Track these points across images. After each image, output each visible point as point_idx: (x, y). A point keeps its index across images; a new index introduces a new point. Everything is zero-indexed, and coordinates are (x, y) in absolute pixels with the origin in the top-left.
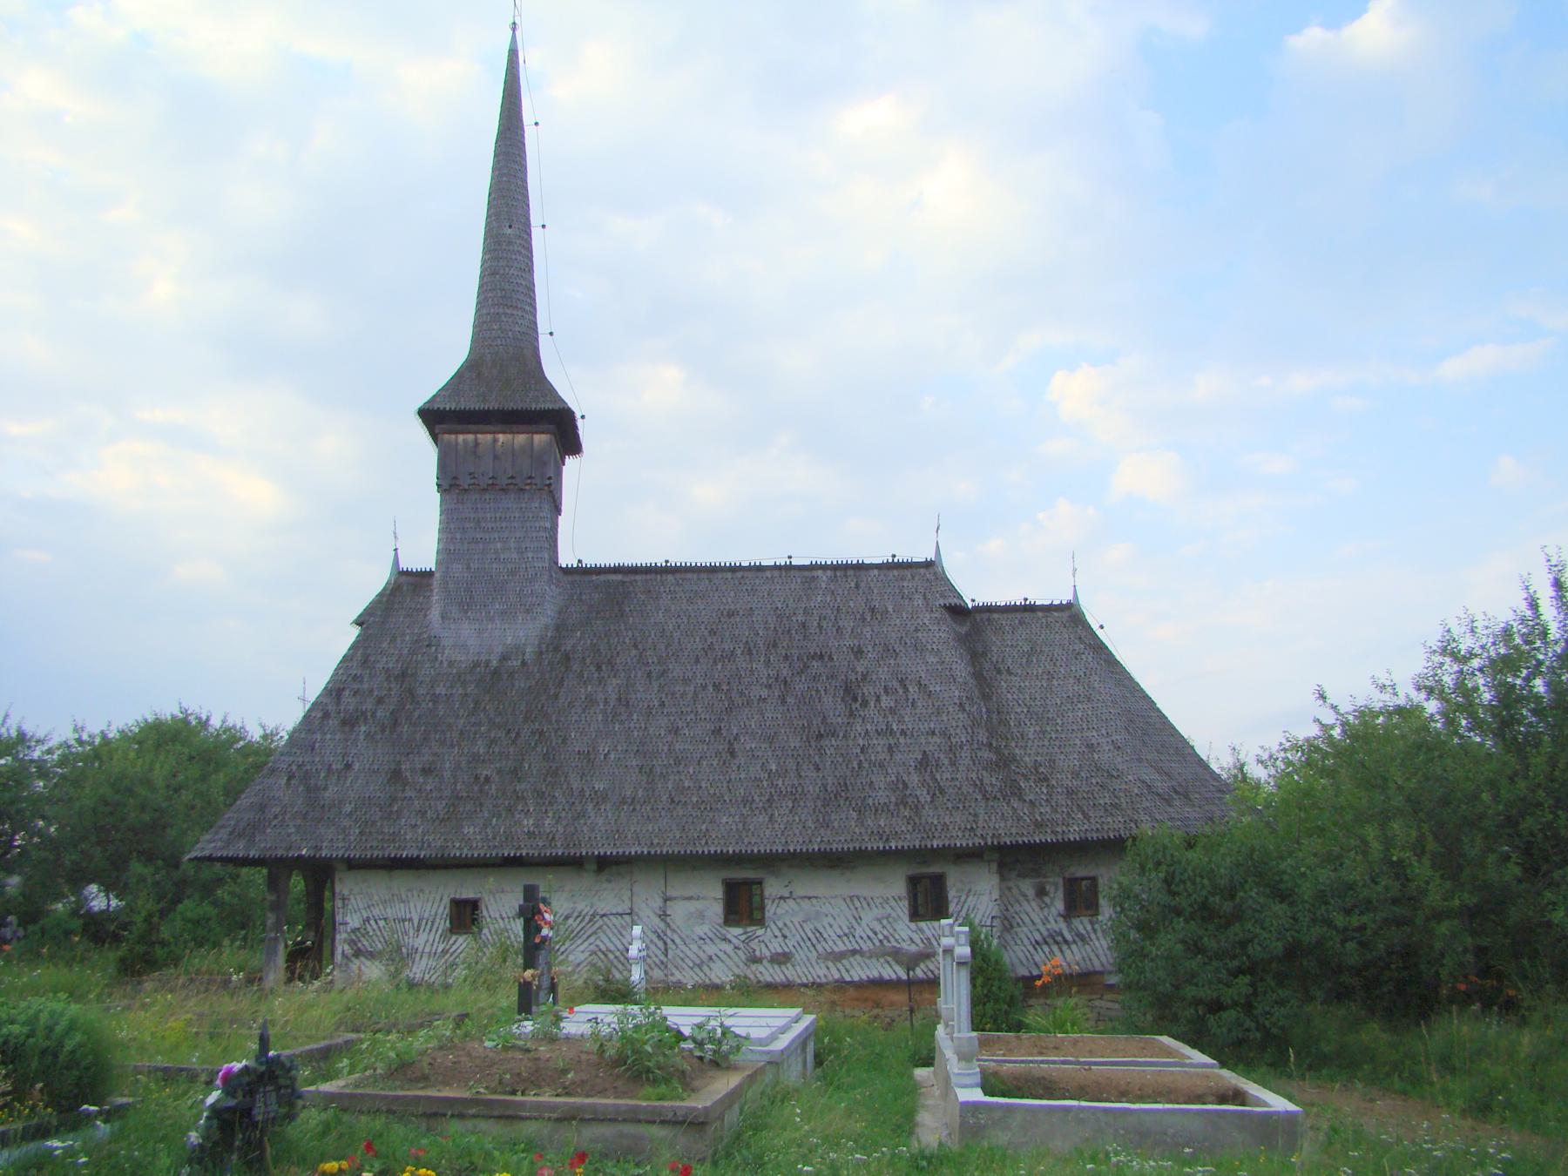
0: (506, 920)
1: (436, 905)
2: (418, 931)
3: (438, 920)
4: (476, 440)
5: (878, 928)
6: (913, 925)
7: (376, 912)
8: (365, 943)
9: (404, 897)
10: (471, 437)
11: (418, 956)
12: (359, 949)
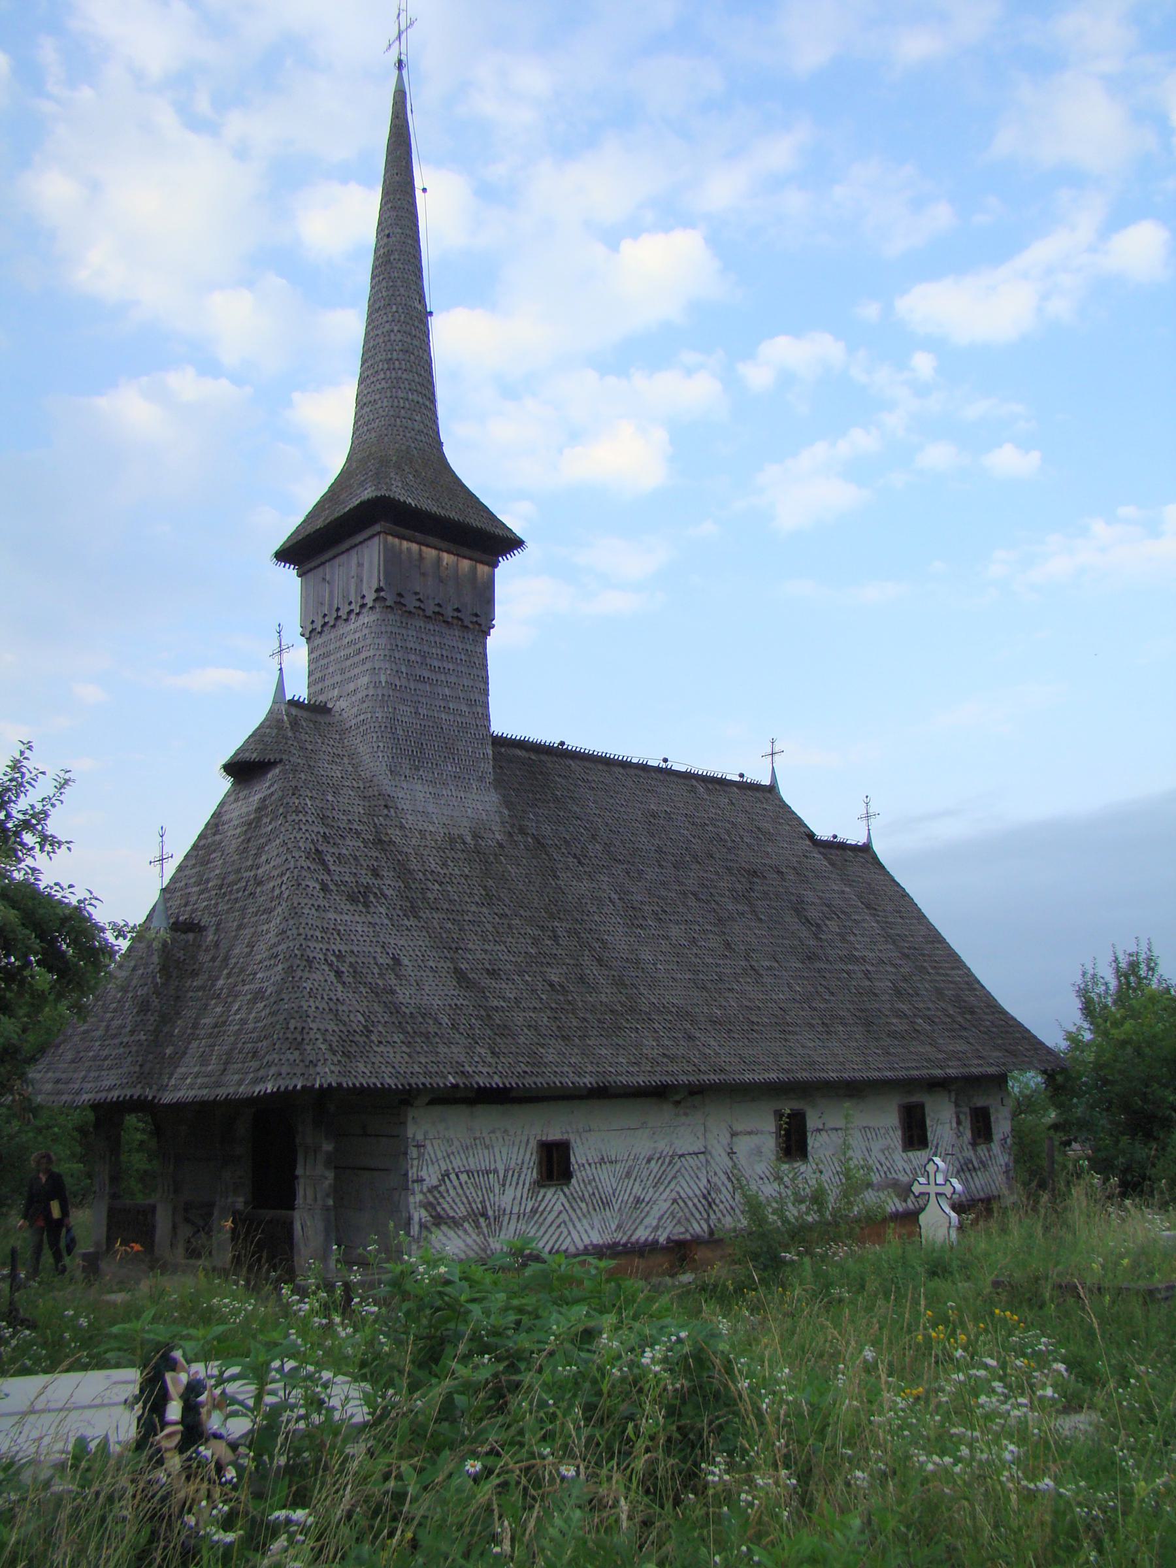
4: (420, 550)
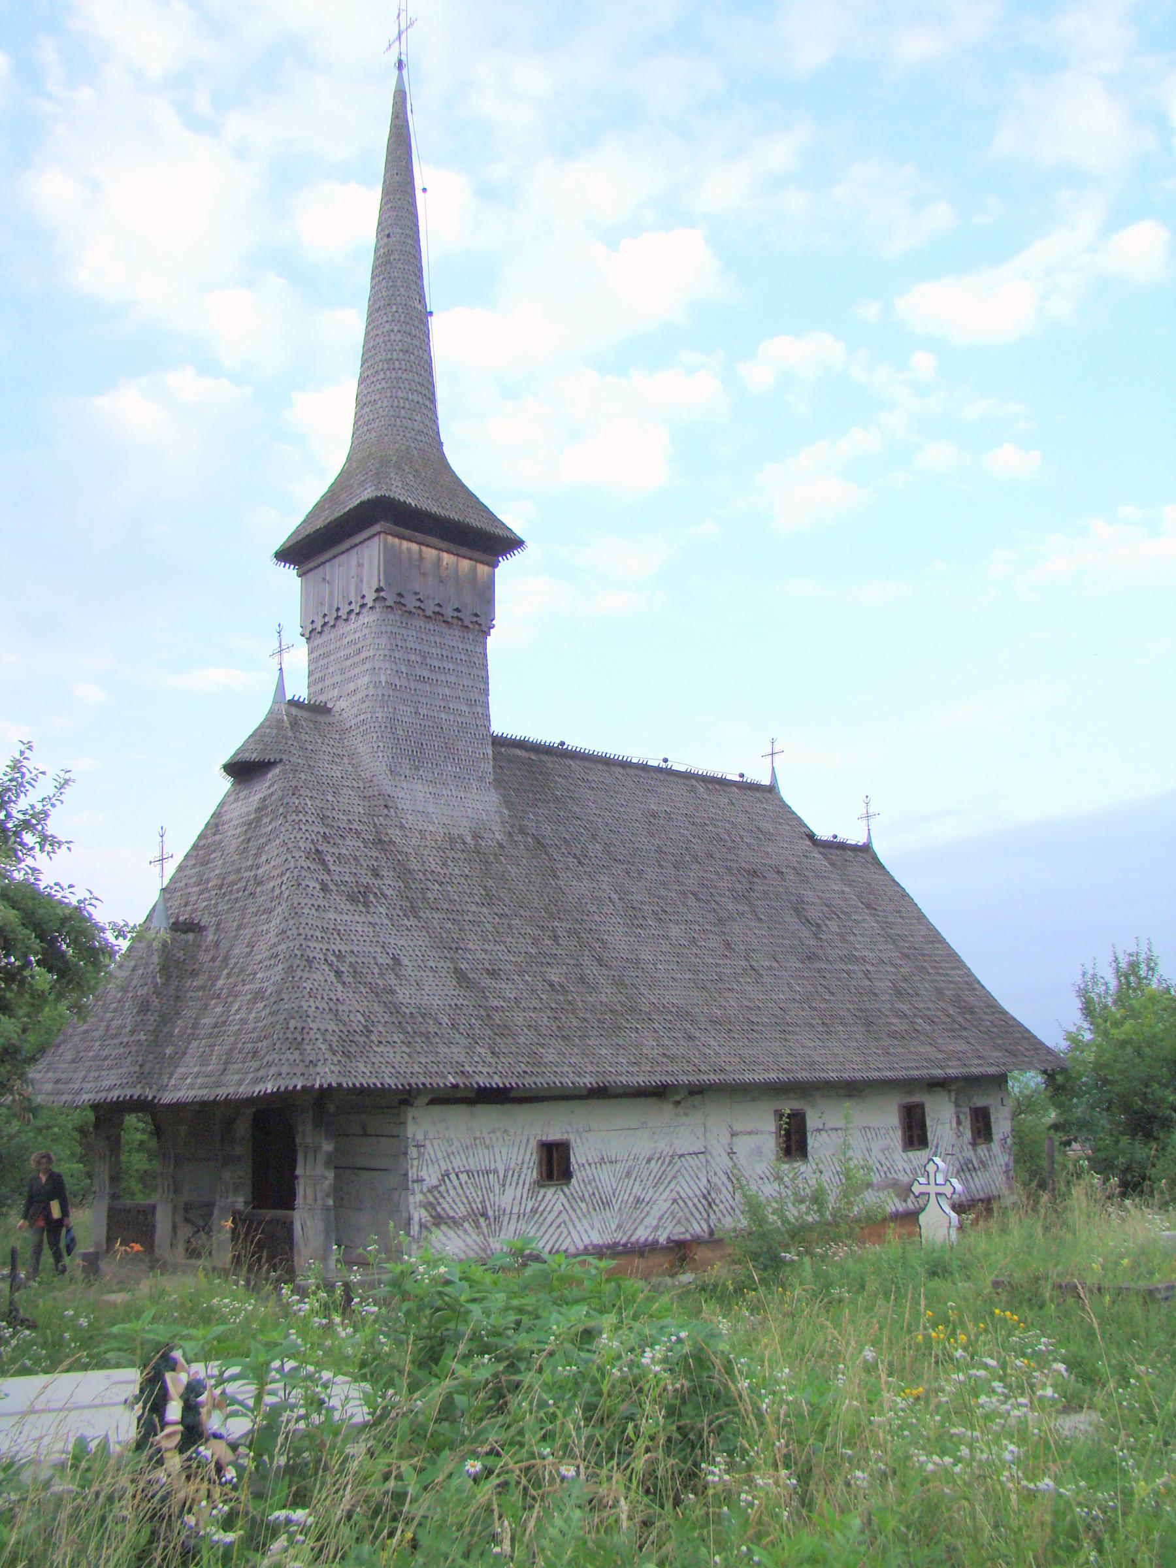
0: (593, 1166)
1: (522, 1150)
2: (504, 1185)
3: (524, 1170)
4: (420, 550)
5: (883, 1160)
6: (904, 1155)
7: (457, 1163)
8: (445, 1206)
9: (488, 1142)
10: (415, 547)
11: (507, 1218)
12: (439, 1216)
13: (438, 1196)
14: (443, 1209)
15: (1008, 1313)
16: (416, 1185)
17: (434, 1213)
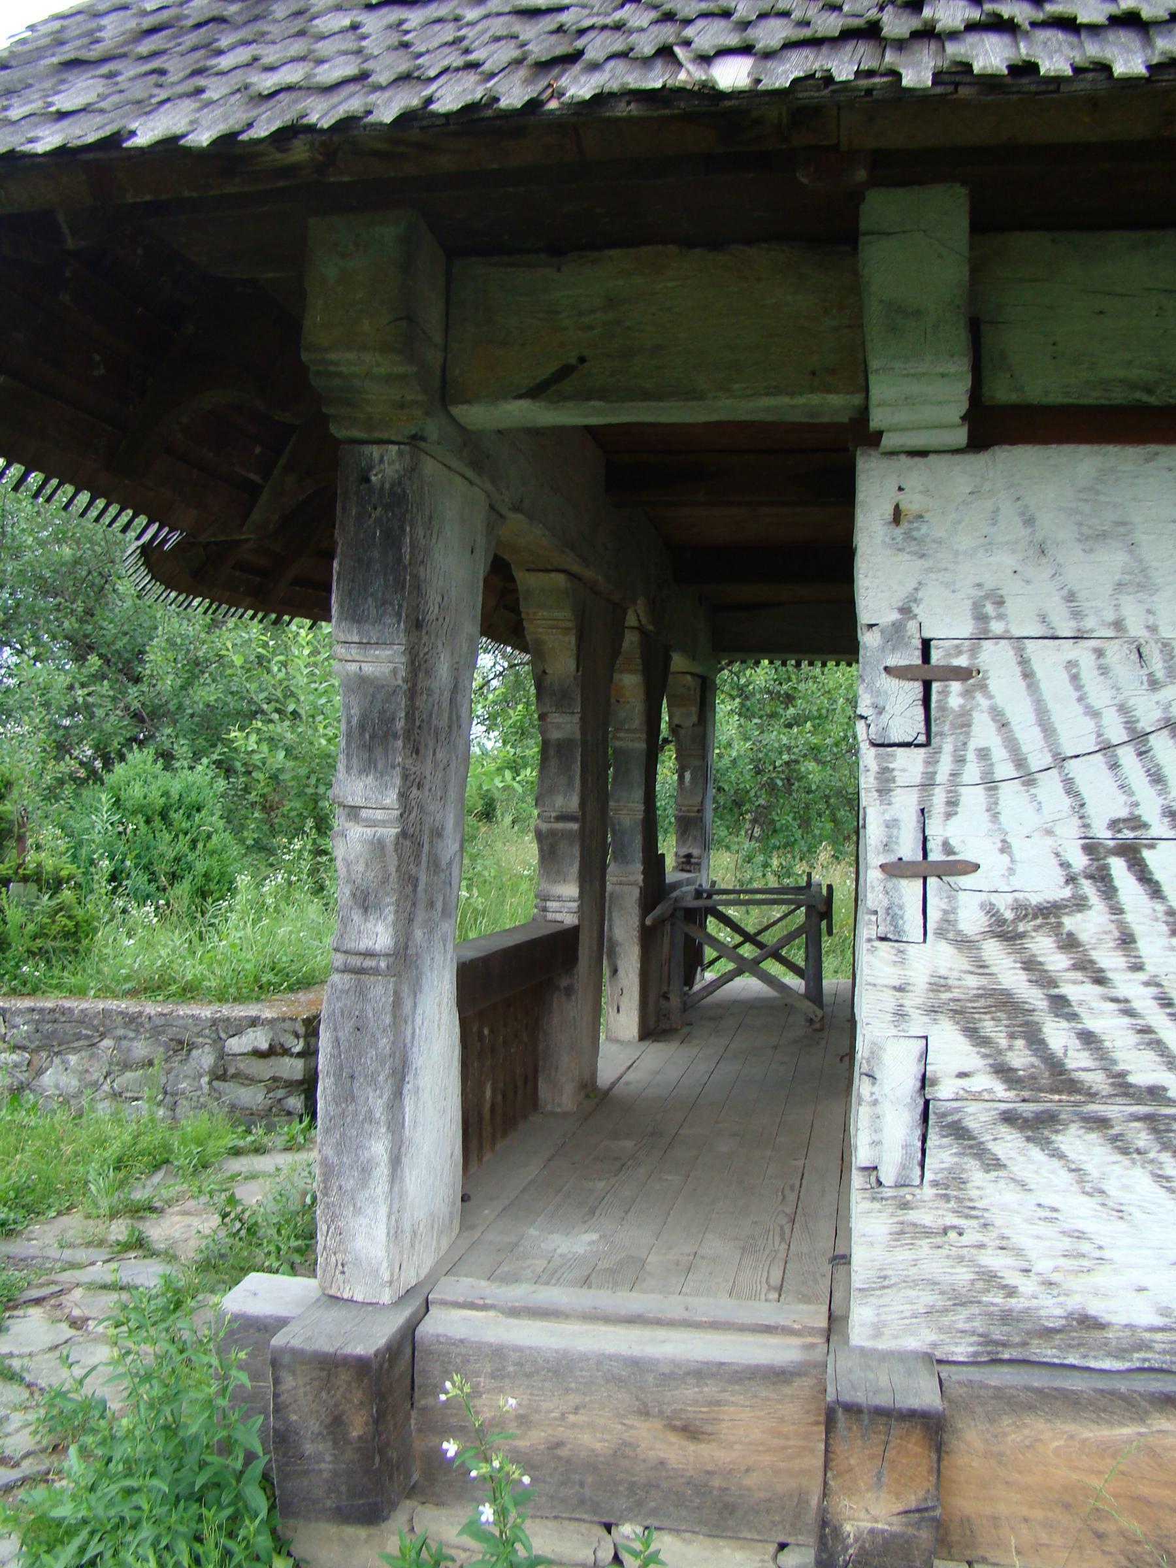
13: (1057, 962)
14: (1088, 1039)
15: (516, 1476)
16: (910, 889)
17: (1020, 1058)
